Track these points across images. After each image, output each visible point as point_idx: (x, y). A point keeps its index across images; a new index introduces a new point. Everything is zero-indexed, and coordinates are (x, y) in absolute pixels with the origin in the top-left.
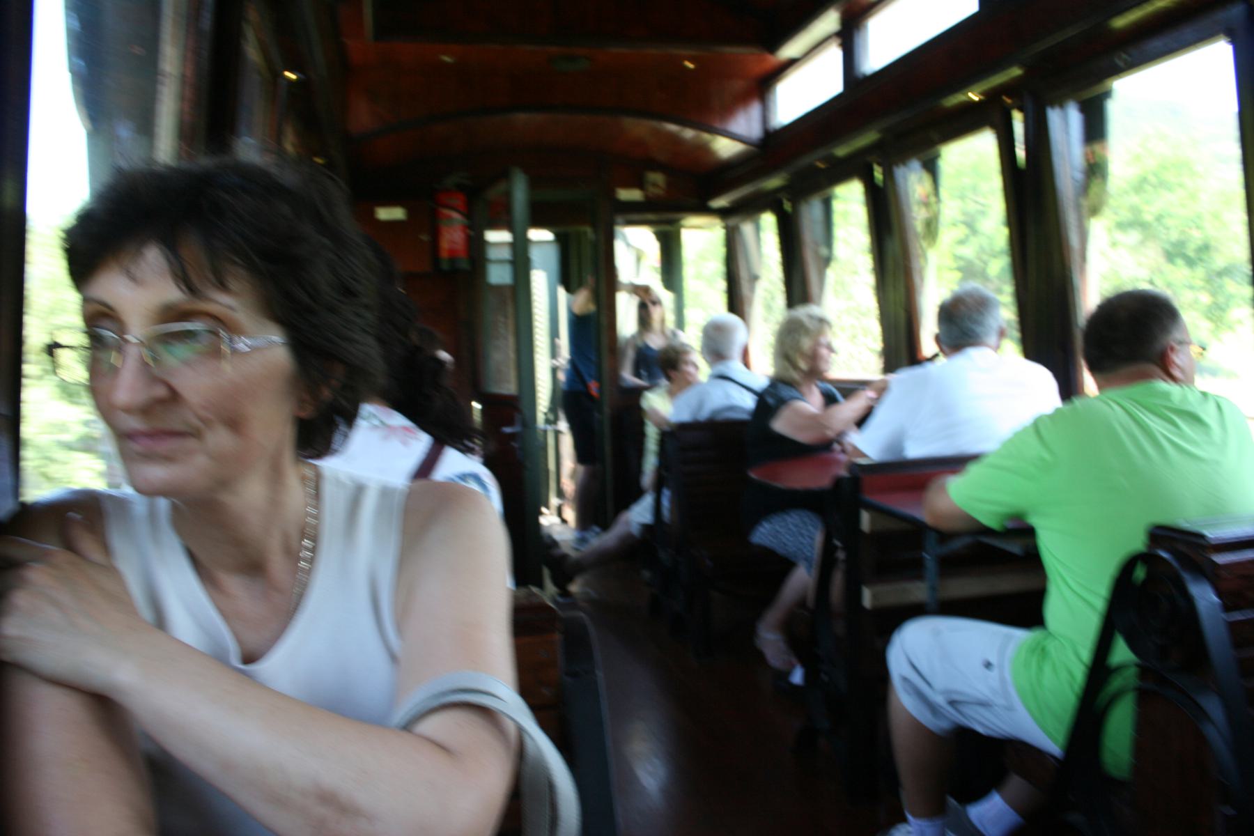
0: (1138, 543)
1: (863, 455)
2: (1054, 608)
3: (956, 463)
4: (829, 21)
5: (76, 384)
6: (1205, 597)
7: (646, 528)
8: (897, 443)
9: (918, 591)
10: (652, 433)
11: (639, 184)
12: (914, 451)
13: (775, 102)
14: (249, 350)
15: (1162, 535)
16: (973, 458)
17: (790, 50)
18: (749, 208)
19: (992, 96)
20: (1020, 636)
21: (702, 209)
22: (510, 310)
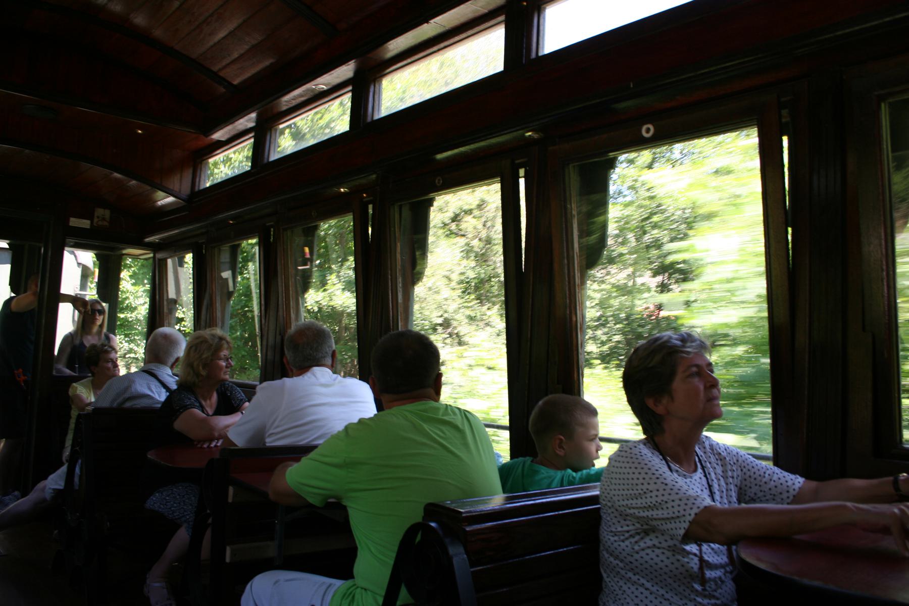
0: (418, 517)
1: (236, 446)
2: (363, 565)
3: (298, 452)
4: (248, 121)
5: (582, 315)
6: (458, 555)
7: (57, 492)
8: (260, 434)
9: (271, 549)
10: (74, 413)
11: (90, 216)
12: (270, 442)
13: (544, 18)
14: (246, 354)
15: (433, 510)
16: (307, 449)
17: (219, 135)
18: (176, 247)
19: (355, 192)
20: (338, 584)
21: (139, 244)
22: (628, 164)
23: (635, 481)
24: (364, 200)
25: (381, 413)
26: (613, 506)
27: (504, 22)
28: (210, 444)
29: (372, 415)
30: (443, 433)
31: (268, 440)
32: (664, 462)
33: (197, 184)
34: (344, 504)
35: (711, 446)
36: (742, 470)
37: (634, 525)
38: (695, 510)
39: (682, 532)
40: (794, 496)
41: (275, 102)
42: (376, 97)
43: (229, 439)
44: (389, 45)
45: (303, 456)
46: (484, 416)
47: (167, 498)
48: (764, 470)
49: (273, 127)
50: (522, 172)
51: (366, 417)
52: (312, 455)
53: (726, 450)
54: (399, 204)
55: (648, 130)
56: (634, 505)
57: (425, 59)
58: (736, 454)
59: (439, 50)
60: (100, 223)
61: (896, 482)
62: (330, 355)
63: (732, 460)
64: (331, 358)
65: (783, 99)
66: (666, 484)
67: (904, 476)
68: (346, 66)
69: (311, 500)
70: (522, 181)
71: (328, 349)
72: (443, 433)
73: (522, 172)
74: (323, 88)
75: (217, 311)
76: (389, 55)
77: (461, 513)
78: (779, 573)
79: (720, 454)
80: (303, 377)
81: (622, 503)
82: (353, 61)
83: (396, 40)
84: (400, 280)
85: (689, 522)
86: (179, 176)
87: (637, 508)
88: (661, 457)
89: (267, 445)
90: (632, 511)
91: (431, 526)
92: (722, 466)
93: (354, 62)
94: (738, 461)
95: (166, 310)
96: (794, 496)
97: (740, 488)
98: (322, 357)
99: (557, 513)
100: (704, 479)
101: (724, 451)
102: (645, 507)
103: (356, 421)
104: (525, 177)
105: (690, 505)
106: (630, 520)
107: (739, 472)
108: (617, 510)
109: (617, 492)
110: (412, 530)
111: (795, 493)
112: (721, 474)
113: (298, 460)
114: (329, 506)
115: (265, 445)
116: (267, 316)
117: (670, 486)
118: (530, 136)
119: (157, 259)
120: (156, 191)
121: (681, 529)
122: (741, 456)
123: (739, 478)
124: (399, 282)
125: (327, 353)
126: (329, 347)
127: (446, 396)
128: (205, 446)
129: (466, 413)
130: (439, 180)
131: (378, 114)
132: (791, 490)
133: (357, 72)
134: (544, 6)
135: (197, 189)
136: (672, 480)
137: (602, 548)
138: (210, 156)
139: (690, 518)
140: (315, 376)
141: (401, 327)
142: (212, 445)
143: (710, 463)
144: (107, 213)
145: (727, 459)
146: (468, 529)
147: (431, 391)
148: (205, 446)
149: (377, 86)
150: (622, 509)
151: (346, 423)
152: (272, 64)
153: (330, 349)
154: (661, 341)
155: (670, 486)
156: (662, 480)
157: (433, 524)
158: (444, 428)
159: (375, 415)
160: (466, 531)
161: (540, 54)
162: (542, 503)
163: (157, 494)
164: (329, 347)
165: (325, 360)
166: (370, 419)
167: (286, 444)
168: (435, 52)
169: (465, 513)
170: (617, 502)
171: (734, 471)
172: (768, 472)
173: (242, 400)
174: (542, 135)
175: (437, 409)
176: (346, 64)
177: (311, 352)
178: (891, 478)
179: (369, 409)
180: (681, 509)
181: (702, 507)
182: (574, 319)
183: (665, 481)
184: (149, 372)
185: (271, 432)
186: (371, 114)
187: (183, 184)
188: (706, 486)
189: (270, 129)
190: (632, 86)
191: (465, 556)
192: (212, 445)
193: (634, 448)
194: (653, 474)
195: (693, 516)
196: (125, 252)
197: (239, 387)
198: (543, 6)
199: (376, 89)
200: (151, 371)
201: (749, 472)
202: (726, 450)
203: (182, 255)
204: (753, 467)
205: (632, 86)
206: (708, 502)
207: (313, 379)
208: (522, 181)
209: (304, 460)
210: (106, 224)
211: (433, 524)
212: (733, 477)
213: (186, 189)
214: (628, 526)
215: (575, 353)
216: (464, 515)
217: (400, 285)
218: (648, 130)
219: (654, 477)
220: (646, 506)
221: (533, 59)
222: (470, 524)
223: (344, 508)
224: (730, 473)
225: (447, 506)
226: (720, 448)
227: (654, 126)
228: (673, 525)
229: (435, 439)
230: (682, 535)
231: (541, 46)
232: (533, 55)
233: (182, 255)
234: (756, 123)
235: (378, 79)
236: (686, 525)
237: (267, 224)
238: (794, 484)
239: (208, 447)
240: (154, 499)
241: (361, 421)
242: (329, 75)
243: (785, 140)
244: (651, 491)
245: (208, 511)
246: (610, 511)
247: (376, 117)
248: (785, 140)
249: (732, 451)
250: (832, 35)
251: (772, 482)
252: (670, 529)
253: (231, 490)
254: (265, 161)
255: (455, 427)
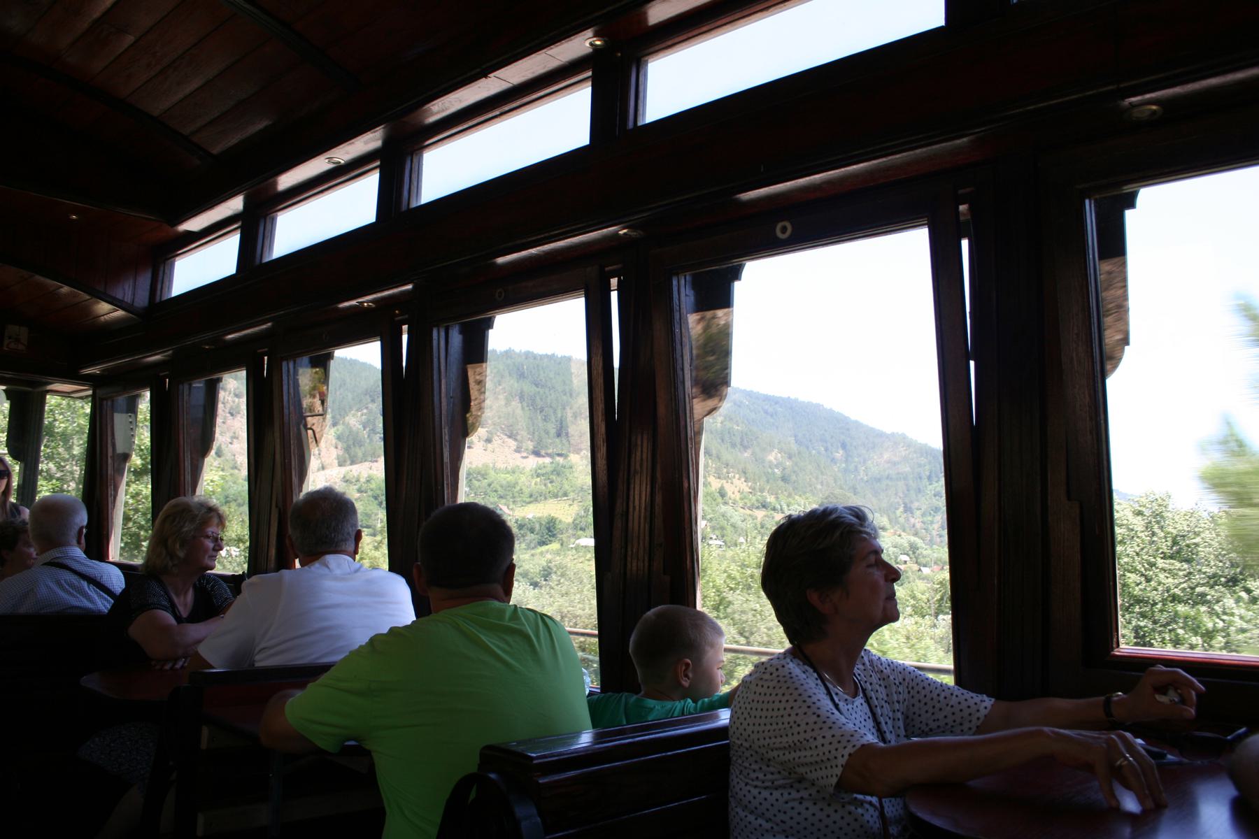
0: (472, 766)
6: (527, 815)
8: (244, 652)
12: (263, 661)
15: (494, 756)
17: (195, 224)
21: (71, 375)
23: (782, 712)
24: (397, 319)
25: (423, 619)
26: (750, 746)
27: (591, 79)
28: (175, 664)
29: (409, 623)
30: (510, 646)
31: (257, 658)
32: (819, 682)
33: (159, 292)
34: (367, 747)
35: (871, 661)
36: (909, 692)
37: (779, 772)
38: (850, 750)
39: (834, 780)
40: (977, 727)
41: (271, 180)
42: (414, 176)
43: (201, 657)
44: (433, 105)
45: (309, 682)
46: (879, 654)
47: (112, 745)
48: (937, 691)
49: (268, 215)
50: (405, 327)
51: (400, 626)
52: (324, 679)
53: (889, 665)
54: (445, 325)
55: (784, 230)
56: (777, 745)
57: (436, 145)
58: (902, 671)
59: (502, 114)
60: (13, 346)
61: (1108, 702)
62: (353, 537)
63: (897, 679)
64: (354, 542)
65: (960, 192)
66: (819, 716)
67: (1118, 695)
68: (372, 133)
69: (321, 744)
70: (614, 296)
71: (350, 529)
72: (510, 646)
73: (405, 327)
74: (340, 162)
75: (186, 473)
76: (432, 119)
77: (533, 758)
78: (960, 832)
79: (882, 671)
80: (310, 568)
81: (762, 742)
82: (383, 126)
83: (442, 98)
84: (446, 430)
85: (842, 766)
86: (131, 282)
87: (780, 749)
88: (815, 675)
89: (257, 665)
90: (775, 753)
91: (490, 778)
92: (886, 687)
93: (383, 128)
94: (904, 680)
95: (110, 471)
96: (977, 727)
97: (907, 717)
98: (342, 540)
99: (664, 754)
100: (865, 705)
101: (888, 667)
102: (785, 748)
103: (385, 631)
104: (619, 290)
105: (844, 743)
106: (774, 767)
107: (906, 696)
108: (756, 752)
109: (756, 728)
110: (464, 784)
111: (979, 723)
112: (885, 698)
113: (302, 686)
114: (346, 751)
115: (253, 665)
116: (258, 482)
117: (823, 718)
118: (625, 234)
119: (97, 398)
120: (98, 303)
121: (831, 776)
122: (910, 673)
123: (906, 703)
124: (445, 434)
125: (348, 534)
126: (352, 527)
127: (522, 595)
128: (167, 667)
129: (545, 617)
130: (500, 293)
131: (643, 120)
132: (974, 719)
133: (387, 142)
134: (646, 58)
135: (158, 300)
136: (828, 711)
137: (733, 803)
138: (170, 256)
139: (842, 761)
140: (328, 568)
141: (448, 501)
142: (178, 666)
143: (871, 684)
144: (23, 332)
145: (892, 678)
146: (540, 781)
147: (499, 590)
148: (167, 667)
149: (415, 160)
150: (763, 751)
151: (372, 634)
152: (266, 127)
153: (354, 528)
154: (834, 516)
155: (823, 718)
156: (814, 709)
157: (493, 776)
158: (509, 639)
159: (413, 622)
160: (539, 783)
161: (640, 123)
162: (643, 740)
163: (97, 739)
164: (352, 527)
165: (346, 544)
166: (406, 627)
167: (279, 664)
168: (496, 117)
169: (538, 758)
170: (756, 741)
171: (900, 693)
172: (943, 695)
173: (227, 599)
174: (641, 233)
175: (501, 613)
176: (372, 131)
177: (328, 533)
178: (1103, 698)
179: (408, 615)
180: (832, 748)
181: (858, 745)
182: (686, 485)
183: (818, 712)
184: (54, 562)
185: (262, 646)
186: (407, 202)
187: (136, 291)
188: (869, 714)
189: (265, 217)
190: (762, 170)
191: (539, 819)
192: (178, 666)
193: (780, 669)
194: (804, 701)
195: (846, 757)
196: (49, 387)
197: (225, 582)
198: (643, 59)
199: (413, 166)
200: (56, 561)
201: (918, 695)
202: (889, 665)
203: (215, 377)
204: (924, 688)
205: (762, 170)
206: (871, 738)
207: (324, 571)
208: (614, 296)
209: (311, 686)
210: (21, 347)
211: (493, 776)
212: (898, 702)
213: (142, 299)
214: (772, 774)
215: (687, 531)
216: (535, 762)
217: (447, 438)
218: (784, 230)
219: (805, 706)
220: (787, 745)
221: (631, 130)
222: (544, 775)
223: (368, 753)
224: (895, 697)
225: (513, 749)
226: (881, 664)
227: (791, 223)
228: (823, 773)
229: (109, 595)
230: (834, 785)
231: (640, 111)
232: (630, 125)
233: (215, 377)
234: (926, 222)
235: (417, 152)
236: (839, 771)
237: (162, 374)
238: (978, 711)
239: (172, 668)
240: (92, 746)
241: (394, 631)
242: (350, 144)
243: (965, 244)
244: (799, 725)
245: (171, 763)
246: (747, 754)
247: (414, 205)
248: (965, 244)
249: (897, 667)
250: (1095, 91)
251: (949, 707)
252: (820, 778)
253: (205, 731)
254: (404, 208)
255: (526, 637)
